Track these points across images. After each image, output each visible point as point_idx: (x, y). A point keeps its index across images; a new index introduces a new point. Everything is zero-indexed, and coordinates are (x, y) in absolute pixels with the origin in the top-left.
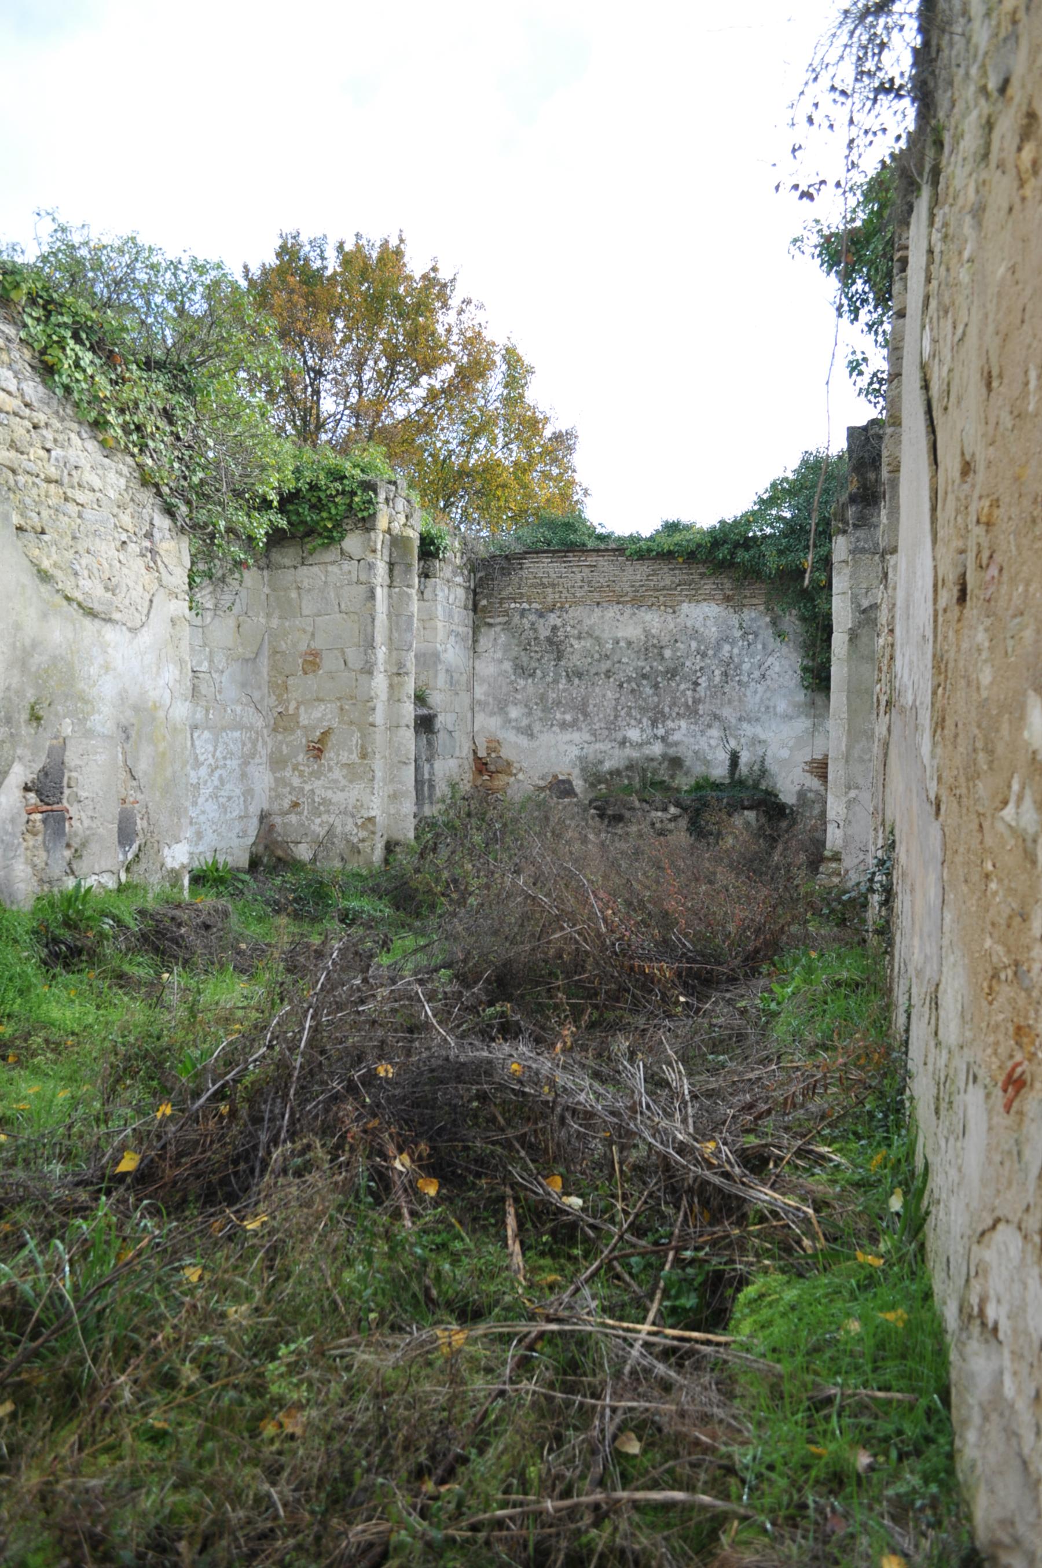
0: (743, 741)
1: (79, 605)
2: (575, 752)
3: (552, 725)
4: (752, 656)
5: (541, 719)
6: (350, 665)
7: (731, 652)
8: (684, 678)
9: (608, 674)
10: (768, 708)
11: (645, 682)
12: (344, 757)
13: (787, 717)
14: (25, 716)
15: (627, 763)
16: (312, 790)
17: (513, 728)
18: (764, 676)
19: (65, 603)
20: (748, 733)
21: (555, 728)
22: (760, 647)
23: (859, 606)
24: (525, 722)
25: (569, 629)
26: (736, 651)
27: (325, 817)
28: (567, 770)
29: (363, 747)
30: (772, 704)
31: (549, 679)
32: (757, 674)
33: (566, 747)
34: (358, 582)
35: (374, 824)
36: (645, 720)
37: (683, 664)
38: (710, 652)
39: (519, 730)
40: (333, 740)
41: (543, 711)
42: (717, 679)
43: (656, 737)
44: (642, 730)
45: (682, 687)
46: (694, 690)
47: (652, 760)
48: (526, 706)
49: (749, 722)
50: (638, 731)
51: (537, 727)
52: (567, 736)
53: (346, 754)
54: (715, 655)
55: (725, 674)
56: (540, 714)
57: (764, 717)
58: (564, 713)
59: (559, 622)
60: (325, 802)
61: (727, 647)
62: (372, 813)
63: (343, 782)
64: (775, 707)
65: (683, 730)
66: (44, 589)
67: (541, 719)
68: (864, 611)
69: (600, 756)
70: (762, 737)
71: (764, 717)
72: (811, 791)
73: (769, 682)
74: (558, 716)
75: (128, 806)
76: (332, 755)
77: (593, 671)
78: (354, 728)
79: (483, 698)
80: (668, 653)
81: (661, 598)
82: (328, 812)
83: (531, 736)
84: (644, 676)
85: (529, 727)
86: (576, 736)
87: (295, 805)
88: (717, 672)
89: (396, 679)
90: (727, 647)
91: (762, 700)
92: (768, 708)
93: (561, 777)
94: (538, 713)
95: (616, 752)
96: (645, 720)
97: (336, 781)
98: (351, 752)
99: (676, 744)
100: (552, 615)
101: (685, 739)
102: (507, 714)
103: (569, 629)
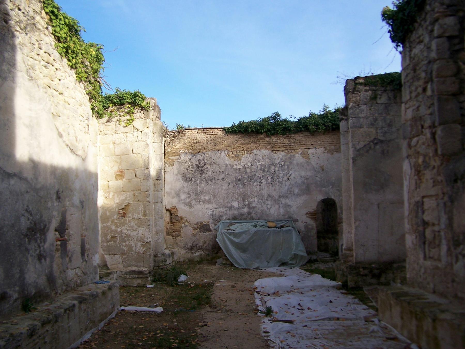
0: (281, 205)
1: (70, 148)
2: (210, 212)
3: (200, 201)
4: (283, 171)
5: (195, 199)
6: (138, 176)
7: (275, 169)
8: (256, 181)
9: (223, 179)
10: (291, 192)
11: (239, 182)
12: (136, 216)
13: (298, 195)
14: (55, 197)
15: (233, 216)
16: (121, 231)
17: (183, 203)
18: (288, 179)
19: (66, 147)
20: (283, 202)
21: (201, 203)
22: (286, 167)
23: (355, 148)
24: (188, 200)
25: (206, 161)
26: (277, 169)
27: (127, 243)
28: (207, 220)
29: (145, 211)
30: (292, 190)
31: (198, 182)
32: (285, 178)
33: (206, 211)
34: (142, 140)
35: (150, 245)
36: (240, 198)
37: (255, 175)
38: (266, 170)
39: (186, 204)
40: (131, 208)
41: (196, 196)
42: (269, 180)
43: (245, 205)
44: (239, 202)
45: (255, 184)
46: (260, 185)
47: (243, 215)
48: (188, 194)
49: (283, 198)
50: (237, 202)
51: (193, 202)
52: (207, 206)
53: (137, 215)
54: (268, 171)
55: (273, 178)
56: (194, 197)
57: (290, 196)
58: (205, 196)
59: (201, 158)
60: (128, 236)
61: (273, 167)
62: (149, 240)
63: (136, 227)
64: (294, 191)
65: (256, 202)
66: (60, 140)
67: (195, 199)
68: (358, 151)
69: (221, 214)
70: (289, 203)
71: (290, 196)
72: (309, 225)
73: (291, 181)
74: (202, 197)
75: (83, 238)
76: (130, 215)
77: (217, 178)
78: (140, 203)
79: (169, 190)
80: (248, 170)
81: (245, 147)
82: (129, 240)
83: (191, 206)
84: (239, 180)
85: (190, 202)
86: (210, 206)
87: (113, 237)
88: (269, 178)
89: (156, 182)
90: (273, 167)
91: (288, 189)
92: (291, 192)
93: (204, 223)
94: (193, 196)
95: (228, 212)
96: (240, 198)
97: (132, 227)
98: (139, 214)
99: (254, 207)
100: (198, 155)
101: (256, 205)
102: (179, 197)
103: (206, 161)
